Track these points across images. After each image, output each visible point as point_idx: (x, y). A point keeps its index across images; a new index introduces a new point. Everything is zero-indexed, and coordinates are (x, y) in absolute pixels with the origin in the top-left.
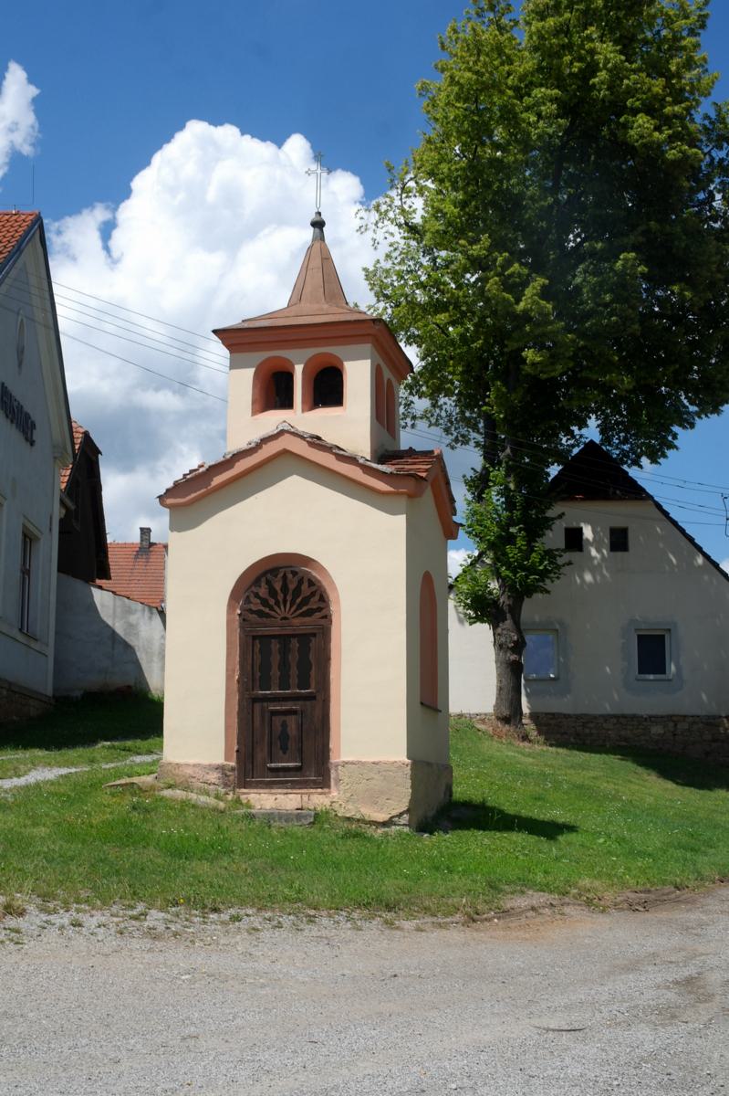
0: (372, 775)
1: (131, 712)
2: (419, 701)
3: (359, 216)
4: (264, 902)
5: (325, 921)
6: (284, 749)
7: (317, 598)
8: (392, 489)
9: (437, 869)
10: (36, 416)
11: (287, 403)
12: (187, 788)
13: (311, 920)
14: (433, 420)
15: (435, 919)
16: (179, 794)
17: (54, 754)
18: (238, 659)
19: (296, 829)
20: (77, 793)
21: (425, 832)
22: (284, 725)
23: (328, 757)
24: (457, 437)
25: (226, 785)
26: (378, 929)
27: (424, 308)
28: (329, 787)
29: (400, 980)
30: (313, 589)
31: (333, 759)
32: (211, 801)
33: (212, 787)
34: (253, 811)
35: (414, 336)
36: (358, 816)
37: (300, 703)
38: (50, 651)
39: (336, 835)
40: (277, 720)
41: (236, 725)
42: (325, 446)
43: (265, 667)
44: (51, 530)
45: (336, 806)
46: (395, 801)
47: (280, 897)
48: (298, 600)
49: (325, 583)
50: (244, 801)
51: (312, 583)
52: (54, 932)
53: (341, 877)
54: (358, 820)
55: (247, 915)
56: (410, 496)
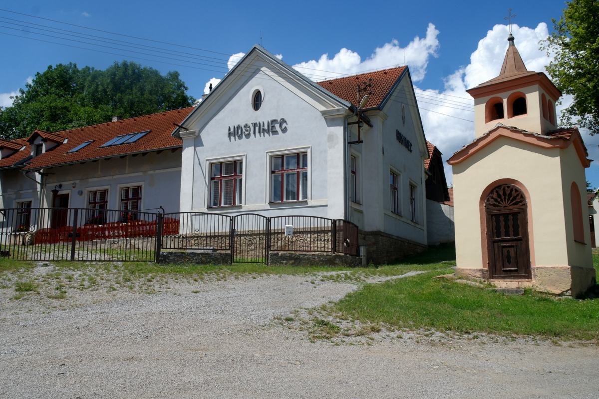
0: (551, 273)
1: (443, 249)
2: (573, 239)
3: (540, 43)
4: (491, 330)
5: (521, 340)
6: (509, 262)
7: (519, 197)
8: (552, 146)
9: (585, 316)
10: (412, 141)
11: (501, 116)
12: (467, 279)
13: (513, 339)
14: (582, 125)
15: (580, 341)
16: (463, 281)
17: (421, 266)
18: (486, 225)
19: (516, 296)
20: (419, 282)
21: (581, 299)
22: (508, 252)
23: (530, 266)
24: (595, 131)
25: (484, 278)
26: (548, 345)
27: (575, 78)
28: (531, 278)
29: (553, 374)
30: (518, 193)
31: (532, 266)
32: (478, 284)
33: (478, 278)
34: (496, 289)
35: (571, 90)
36: (546, 291)
37: (515, 242)
38: (425, 228)
39: (535, 299)
40: (505, 250)
41: (487, 252)
42: (518, 131)
43: (498, 227)
44: (421, 183)
45: (535, 287)
46: (565, 284)
47: (500, 328)
48: (511, 199)
49: (523, 190)
50: (493, 285)
51: (517, 190)
52: (388, 339)
53: (539, 320)
54: (546, 293)
55: (482, 336)
56: (561, 148)
